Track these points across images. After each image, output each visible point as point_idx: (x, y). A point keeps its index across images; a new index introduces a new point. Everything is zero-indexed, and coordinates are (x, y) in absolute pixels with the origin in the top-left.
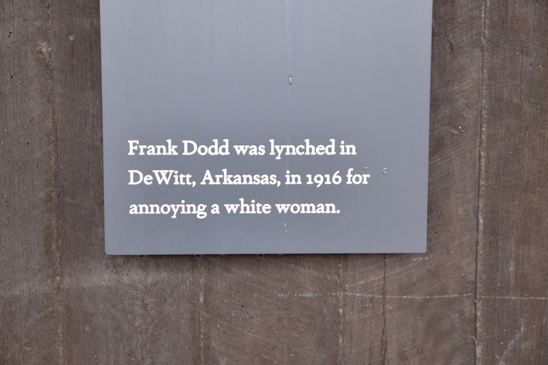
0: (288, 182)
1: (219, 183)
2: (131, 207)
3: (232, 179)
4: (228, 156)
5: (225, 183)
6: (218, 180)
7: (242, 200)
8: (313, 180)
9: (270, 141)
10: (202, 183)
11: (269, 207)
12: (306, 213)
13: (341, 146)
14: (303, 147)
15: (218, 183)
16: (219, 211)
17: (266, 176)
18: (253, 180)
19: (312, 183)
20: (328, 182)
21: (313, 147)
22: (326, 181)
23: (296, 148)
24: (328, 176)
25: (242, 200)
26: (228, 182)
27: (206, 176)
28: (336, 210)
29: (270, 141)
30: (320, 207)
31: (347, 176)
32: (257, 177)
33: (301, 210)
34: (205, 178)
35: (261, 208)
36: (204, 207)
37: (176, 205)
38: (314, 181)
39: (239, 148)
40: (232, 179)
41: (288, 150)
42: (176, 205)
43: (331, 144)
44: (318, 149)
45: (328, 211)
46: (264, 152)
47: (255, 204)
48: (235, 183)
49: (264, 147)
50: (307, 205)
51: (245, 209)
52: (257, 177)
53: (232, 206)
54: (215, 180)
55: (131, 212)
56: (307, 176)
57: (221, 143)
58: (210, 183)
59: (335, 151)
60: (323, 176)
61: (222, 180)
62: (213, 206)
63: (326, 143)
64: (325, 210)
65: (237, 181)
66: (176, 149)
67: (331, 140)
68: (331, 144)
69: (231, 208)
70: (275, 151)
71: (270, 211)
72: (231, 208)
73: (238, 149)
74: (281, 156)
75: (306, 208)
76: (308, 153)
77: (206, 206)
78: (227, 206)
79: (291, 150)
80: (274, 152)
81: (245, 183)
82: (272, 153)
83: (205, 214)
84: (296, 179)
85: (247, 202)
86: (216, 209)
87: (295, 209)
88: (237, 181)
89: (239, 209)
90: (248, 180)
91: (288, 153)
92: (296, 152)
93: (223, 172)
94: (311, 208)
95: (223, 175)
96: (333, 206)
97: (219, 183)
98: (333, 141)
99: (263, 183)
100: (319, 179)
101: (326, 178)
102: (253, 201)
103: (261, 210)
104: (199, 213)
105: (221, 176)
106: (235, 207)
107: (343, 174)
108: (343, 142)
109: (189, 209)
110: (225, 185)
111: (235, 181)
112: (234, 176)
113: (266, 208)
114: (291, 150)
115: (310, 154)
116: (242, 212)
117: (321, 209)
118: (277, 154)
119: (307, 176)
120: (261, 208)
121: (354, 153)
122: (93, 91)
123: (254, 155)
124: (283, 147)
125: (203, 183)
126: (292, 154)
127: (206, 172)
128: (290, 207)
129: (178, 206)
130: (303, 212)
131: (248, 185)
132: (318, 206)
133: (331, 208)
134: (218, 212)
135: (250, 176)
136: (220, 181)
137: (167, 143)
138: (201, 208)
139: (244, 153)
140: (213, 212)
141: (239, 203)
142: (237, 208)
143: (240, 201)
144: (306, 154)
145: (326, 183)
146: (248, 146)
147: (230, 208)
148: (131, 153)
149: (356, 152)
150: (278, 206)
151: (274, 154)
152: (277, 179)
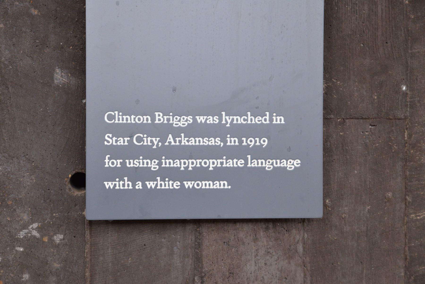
0: (229, 144)
5: (183, 144)
6: (177, 141)
7: (159, 178)
8: (246, 142)
10: (166, 144)
11: (179, 184)
14: (246, 118)
15: (178, 144)
16: (142, 187)
17: (213, 139)
18: (203, 142)
21: (253, 118)
24: (257, 139)
25: (159, 178)
26: (185, 143)
27: (169, 138)
28: (228, 186)
30: (177, 162)
31: (105, 161)
32: (206, 140)
33: (202, 186)
34: (168, 140)
35: (173, 185)
36: (157, 161)
39: (200, 118)
40: (188, 141)
43: (266, 116)
44: (257, 119)
45: (222, 187)
46: (218, 121)
47: (169, 181)
48: (190, 144)
49: (217, 117)
50: (206, 182)
51: (161, 185)
52: (206, 140)
53: (151, 183)
56: (243, 139)
60: (254, 139)
61: (180, 142)
62: (137, 183)
63: (263, 115)
64: (220, 186)
68: (266, 116)
69: (150, 185)
71: (179, 187)
72: (150, 185)
75: (206, 184)
76: (249, 122)
77: (158, 161)
78: (147, 183)
79: (237, 120)
80: (225, 121)
82: (224, 122)
83: (157, 167)
84: (235, 142)
85: (163, 180)
86: (139, 186)
87: (198, 185)
89: (157, 185)
91: (235, 122)
92: (241, 121)
94: (209, 184)
96: (226, 183)
98: (268, 113)
99: (210, 144)
100: (251, 141)
101: (257, 140)
102: (167, 179)
103: (173, 186)
104: (153, 166)
105: (180, 139)
106: (154, 184)
108: (229, 136)
109: (233, 142)
110: (183, 146)
111: (190, 142)
113: (176, 185)
115: (161, 188)
116: (159, 187)
117: (218, 185)
119: (243, 139)
120: (173, 185)
121: (283, 122)
123: (210, 123)
124: (231, 117)
125: (167, 144)
126: (128, 122)
127: (169, 136)
128: (194, 184)
129: (114, 183)
130: (204, 187)
131: (170, 167)
132: (215, 183)
133: (224, 185)
134: (141, 188)
136: (179, 143)
138: (155, 162)
140: (137, 187)
141: (157, 180)
142: (155, 184)
143: (157, 179)
145: (256, 144)
146: (206, 117)
147: (150, 184)
150: (185, 183)
151: (225, 122)
152: (221, 141)
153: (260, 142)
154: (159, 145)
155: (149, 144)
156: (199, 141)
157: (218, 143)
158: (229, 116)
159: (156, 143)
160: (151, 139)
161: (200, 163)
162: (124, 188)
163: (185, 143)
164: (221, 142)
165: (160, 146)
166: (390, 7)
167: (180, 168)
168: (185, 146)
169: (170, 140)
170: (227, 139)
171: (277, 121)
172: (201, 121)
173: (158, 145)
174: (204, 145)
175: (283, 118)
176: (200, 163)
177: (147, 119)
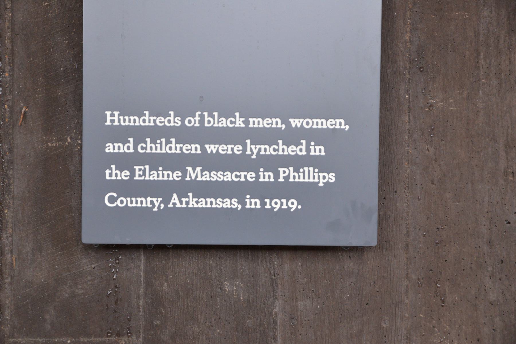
0: (248, 206)
1: (185, 206)
2: (107, 145)
3: (197, 202)
4: (133, 153)
5: (190, 206)
6: (184, 203)
8: (270, 204)
9: (247, 141)
10: (169, 206)
11: (254, 175)
12: (256, 208)
13: (311, 147)
14: (276, 147)
15: (184, 205)
18: (216, 204)
19: (270, 207)
20: (285, 207)
21: (285, 147)
22: (283, 205)
23: (270, 148)
24: (284, 201)
26: (193, 205)
27: (173, 199)
29: (247, 141)
31: (199, 118)
34: (172, 201)
37: (157, 199)
38: (271, 204)
40: (197, 202)
41: (263, 150)
42: (157, 199)
48: (199, 206)
50: (318, 120)
51: (151, 148)
54: (181, 203)
55: (107, 150)
56: (266, 200)
57: (168, 142)
58: (177, 206)
59: (306, 151)
61: (187, 203)
65: (202, 204)
66: (243, 122)
67: (129, 139)
70: (251, 150)
73: (209, 148)
74: (256, 155)
75: (317, 123)
76: (281, 153)
79: (265, 150)
81: (209, 206)
82: (248, 152)
85: (153, 142)
87: (308, 123)
88: (202, 204)
90: (211, 203)
91: (262, 152)
93: (189, 196)
94: (322, 123)
95: (189, 198)
96: (342, 121)
97: (185, 206)
99: (226, 179)
100: (276, 203)
105: (187, 199)
107: (257, 173)
110: (191, 208)
111: (199, 204)
112: (198, 199)
114: (265, 150)
118: (253, 153)
119: (266, 200)
121: (323, 153)
122: (6, 274)
124: (258, 147)
125: (171, 205)
127: (173, 196)
128: (303, 122)
130: (315, 126)
135: (213, 200)
137: (147, 142)
139: (214, 151)
144: (147, 152)
145: (283, 207)
148: (108, 123)
149: (325, 152)
152: (239, 203)
153: (287, 205)
154: (161, 207)
155: (149, 205)
156: (211, 203)
157: (234, 205)
158: (256, 145)
159: (157, 204)
160: (151, 199)
161: (232, 149)
162: (111, 179)
163: (193, 205)
164: (238, 204)
165: (162, 208)
166: (393, 332)
167: (119, 115)
168: (193, 208)
169: (174, 201)
170: (246, 200)
171: (315, 152)
172: (296, 125)
173: (159, 206)
174: (217, 208)
175: (322, 148)
176: (232, 149)
177: (196, 149)
